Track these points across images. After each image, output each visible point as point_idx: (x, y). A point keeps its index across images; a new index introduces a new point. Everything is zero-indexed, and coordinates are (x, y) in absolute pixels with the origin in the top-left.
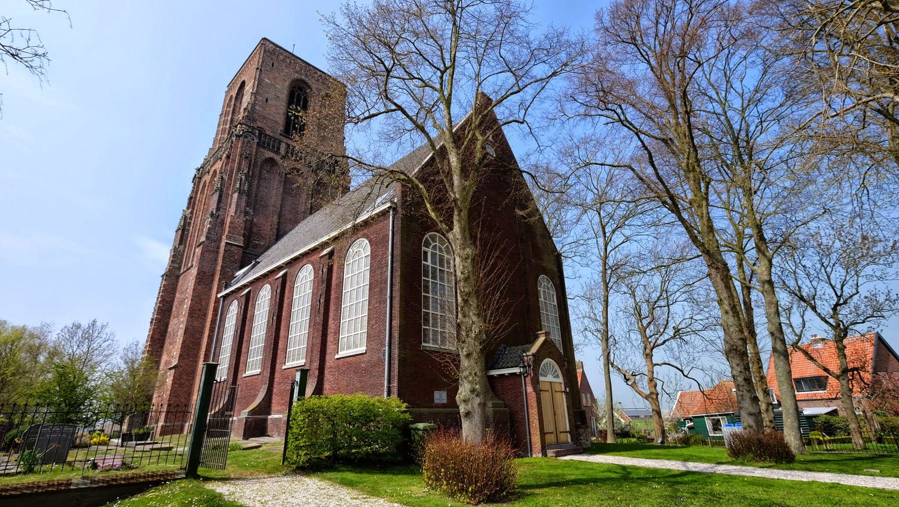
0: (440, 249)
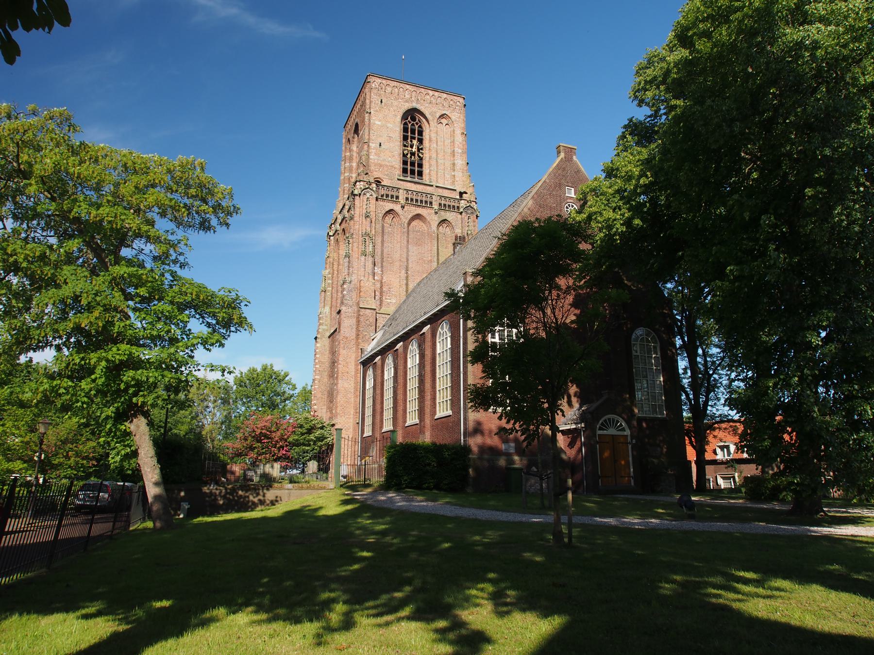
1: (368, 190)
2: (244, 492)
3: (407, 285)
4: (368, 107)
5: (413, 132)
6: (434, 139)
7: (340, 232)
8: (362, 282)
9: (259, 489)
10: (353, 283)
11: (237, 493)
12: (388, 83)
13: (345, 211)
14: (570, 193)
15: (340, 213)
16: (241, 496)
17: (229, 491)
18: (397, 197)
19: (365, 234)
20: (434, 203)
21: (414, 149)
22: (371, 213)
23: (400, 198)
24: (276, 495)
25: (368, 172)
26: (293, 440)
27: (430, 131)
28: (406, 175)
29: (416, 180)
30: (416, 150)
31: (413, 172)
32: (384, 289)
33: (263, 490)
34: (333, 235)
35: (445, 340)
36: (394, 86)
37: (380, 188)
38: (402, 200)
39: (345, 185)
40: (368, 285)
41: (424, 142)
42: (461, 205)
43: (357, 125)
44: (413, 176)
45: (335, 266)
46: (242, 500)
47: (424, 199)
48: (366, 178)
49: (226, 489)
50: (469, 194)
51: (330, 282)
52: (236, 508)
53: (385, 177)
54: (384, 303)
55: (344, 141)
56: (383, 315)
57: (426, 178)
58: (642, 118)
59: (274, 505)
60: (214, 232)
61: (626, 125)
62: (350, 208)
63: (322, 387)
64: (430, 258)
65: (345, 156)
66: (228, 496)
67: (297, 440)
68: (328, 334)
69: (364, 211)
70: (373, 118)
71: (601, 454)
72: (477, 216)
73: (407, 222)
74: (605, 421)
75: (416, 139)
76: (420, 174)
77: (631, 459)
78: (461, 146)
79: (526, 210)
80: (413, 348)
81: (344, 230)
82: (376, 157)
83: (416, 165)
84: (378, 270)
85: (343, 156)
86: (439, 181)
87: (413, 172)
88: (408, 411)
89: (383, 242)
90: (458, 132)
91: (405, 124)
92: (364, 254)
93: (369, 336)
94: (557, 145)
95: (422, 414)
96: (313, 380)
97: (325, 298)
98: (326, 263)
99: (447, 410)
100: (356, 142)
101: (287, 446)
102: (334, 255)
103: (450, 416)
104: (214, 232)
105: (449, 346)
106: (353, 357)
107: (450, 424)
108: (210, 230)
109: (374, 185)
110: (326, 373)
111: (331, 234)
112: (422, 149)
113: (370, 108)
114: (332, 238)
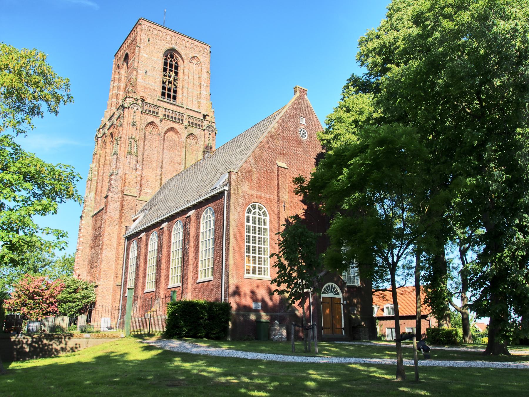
0: (259, 214)
1: (136, 105)
2: (48, 341)
3: (161, 180)
4: (138, 42)
5: (171, 66)
6: (186, 73)
7: (108, 135)
8: (127, 175)
9: (62, 338)
10: (119, 175)
11: (42, 342)
12: (155, 27)
13: (114, 119)
14: (302, 121)
15: (109, 120)
16: (46, 344)
17: (35, 340)
18: (157, 113)
19: (132, 138)
20: (184, 120)
21: (172, 79)
22: (137, 123)
23: (160, 113)
24: (76, 342)
25: (136, 91)
26: (62, 297)
27: (184, 67)
28: (164, 97)
29: (171, 102)
30: (173, 80)
31: (169, 96)
32: (143, 182)
33: (65, 339)
34: (101, 137)
35: (208, 222)
36: (159, 30)
37: (145, 104)
38: (161, 116)
39: (113, 100)
40: (132, 177)
41: (179, 75)
42: (204, 124)
43: (127, 56)
44: (169, 99)
45: (102, 162)
46: (46, 348)
47: (177, 117)
48: (134, 96)
49: (33, 338)
50: (210, 116)
51: (96, 173)
52: (41, 354)
53: (148, 97)
54: (143, 193)
55: (114, 66)
56: (142, 202)
57: (179, 101)
58: (361, 75)
59: (74, 351)
60: (42, 117)
61: (349, 79)
62: (119, 117)
63: (84, 256)
64: (179, 161)
65: (114, 78)
66: (34, 344)
67: (65, 298)
68: (92, 214)
69: (132, 121)
70: (142, 51)
71: (324, 311)
72: (216, 134)
73: (163, 132)
74: (327, 287)
75: (173, 71)
76: (175, 98)
77: (343, 315)
78: (206, 81)
79: (273, 130)
80: (178, 227)
81: (111, 134)
82: (142, 81)
83: (172, 91)
84: (139, 166)
85: (113, 77)
86: (188, 105)
87: (169, 96)
88: (170, 276)
89: (144, 145)
90: (205, 71)
91: (166, 59)
92: (130, 153)
93: (130, 217)
94: (294, 86)
95: (185, 279)
96: (77, 250)
97: (91, 186)
98: (93, 159)
99: (208, 276)
100: (124, 68)
101: (55, 302)
102: (101, 153)
103: (212, 280)
104: (42, 117)
105: (212, 227)
106: (117, 233)
107: (212, 287)
108: (38, 115)
109: (140, 102)
110: (88, 245)
111: (99, 136)
112: (177, 79)
113: (140, 43)
114: (99, 139)
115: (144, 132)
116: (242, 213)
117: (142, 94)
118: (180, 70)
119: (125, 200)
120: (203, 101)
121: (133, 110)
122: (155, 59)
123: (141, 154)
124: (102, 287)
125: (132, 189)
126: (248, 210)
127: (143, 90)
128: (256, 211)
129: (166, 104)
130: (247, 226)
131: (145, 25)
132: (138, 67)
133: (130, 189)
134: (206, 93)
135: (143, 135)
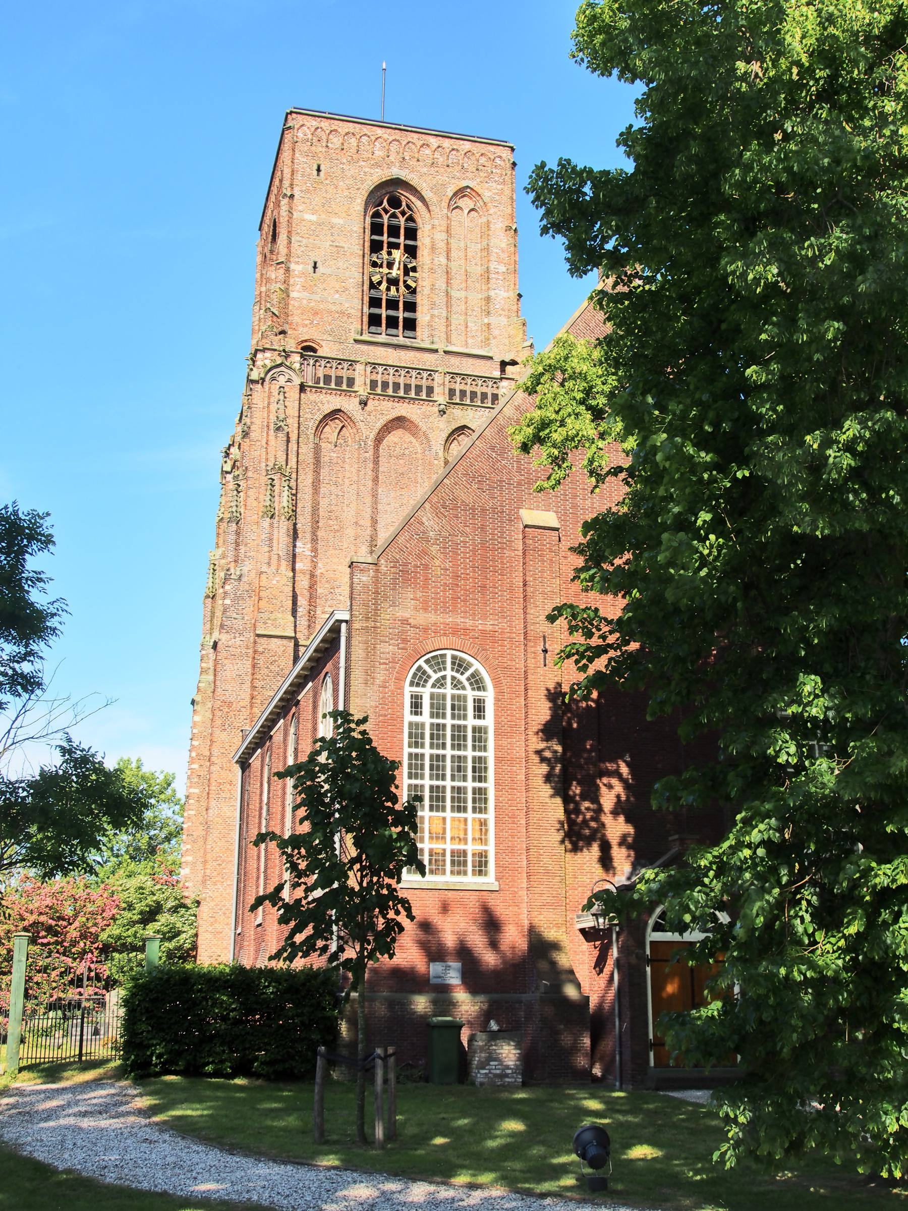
0: (457, 684)
1: (282, 369)
8: (263, 576)
10: (244, 579)
12: (334, 127)
18: (351, 382)
20: (436, 390)
25: (286, 327)
28: (379, 330)
29: (401, 340)
30: (401, 272)
32: (320, 591)
36: (347, 134)
38: (361, 388)
57: (422, 336)
73: (372, 436)
75: (402, 247)
76: (411, 325)
78: (504, 256)
83: (401, 305)
113: (292, 185)
115: (311, 446)
116: (392, 687)
117: (306, 333)
118: (423, 241)
119: (260, 649)
120: (499, 321)
121: (275, 387)
122: (341, 222)
123: (309, 509)
124: (212, 904)
125: (280, 615)
126: (415, 675)
127: (307, 322)
128: (444, 677)
129: (382, 350)
130: (411, 724)
131: (304, 127)
132: (288, 255)
133: (273, 616)
134: (505, 295)
135: (311, 455)
